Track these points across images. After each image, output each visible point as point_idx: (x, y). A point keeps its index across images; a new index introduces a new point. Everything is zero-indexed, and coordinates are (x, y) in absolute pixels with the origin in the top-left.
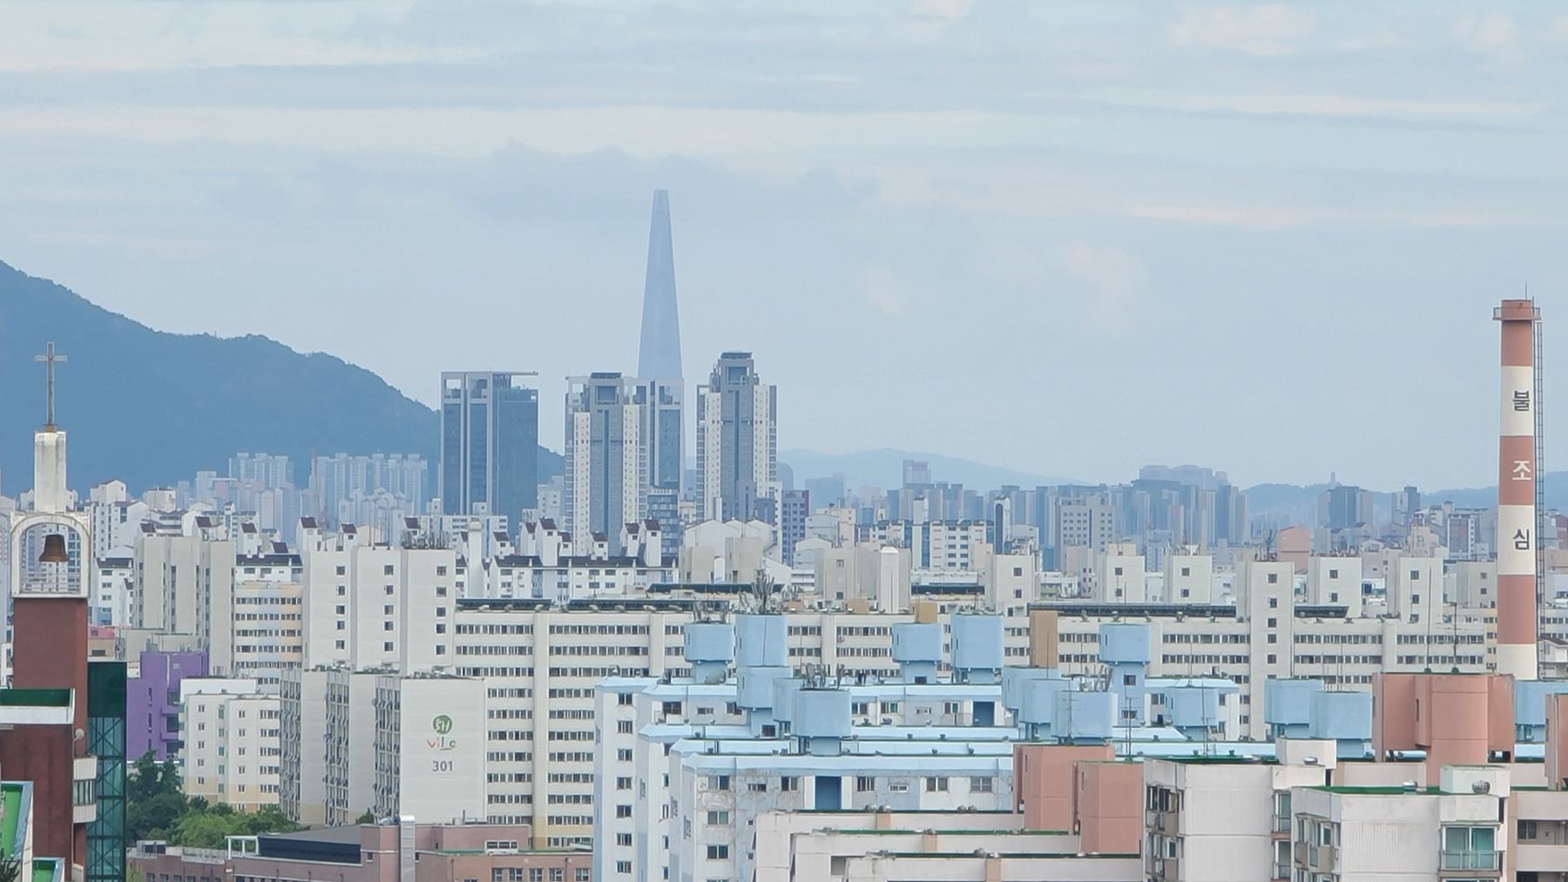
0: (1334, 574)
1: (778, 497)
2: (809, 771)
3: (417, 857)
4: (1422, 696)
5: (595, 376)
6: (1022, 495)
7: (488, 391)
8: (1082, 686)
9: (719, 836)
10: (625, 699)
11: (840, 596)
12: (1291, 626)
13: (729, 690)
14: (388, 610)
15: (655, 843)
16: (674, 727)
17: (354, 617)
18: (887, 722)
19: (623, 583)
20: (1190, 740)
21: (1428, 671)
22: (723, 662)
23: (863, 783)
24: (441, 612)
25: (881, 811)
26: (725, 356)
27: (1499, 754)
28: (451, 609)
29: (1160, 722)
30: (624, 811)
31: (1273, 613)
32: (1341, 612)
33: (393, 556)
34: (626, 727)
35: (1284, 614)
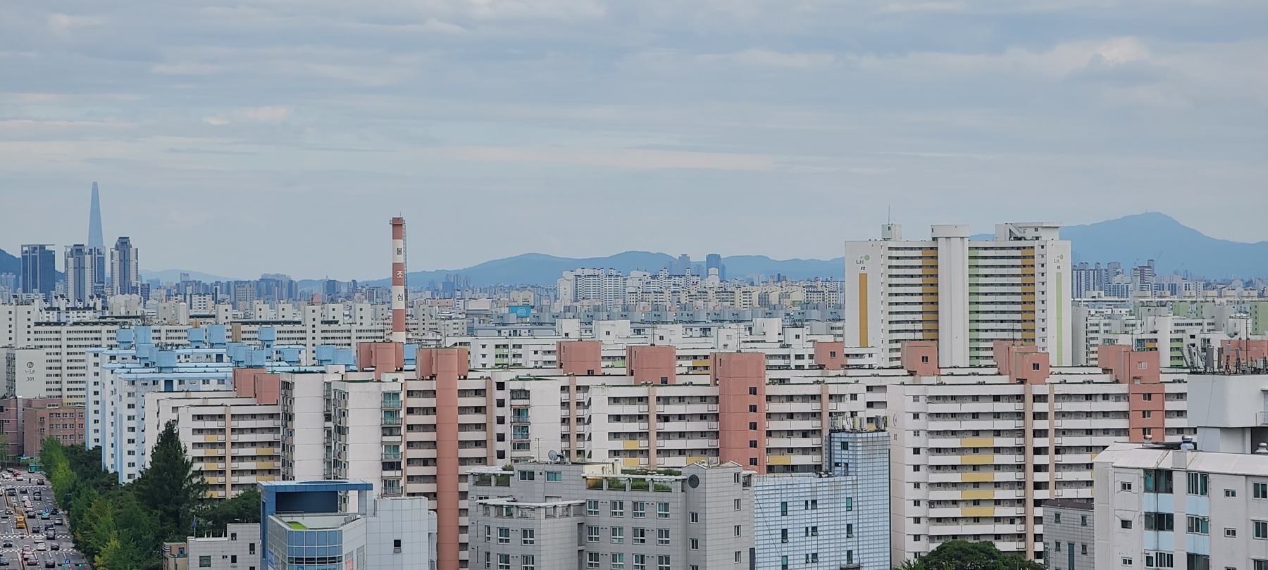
0: (361, 309)
1: (139, 286)
2: (163, 378)
3: (23, 410)
4: (373, 350)
5: (75, 245)
6: (222, 285)
7: (37, 251)
8: (255, 348)
9: (132, 401)
10: (96, 355)
11: (165, 319)
12: (320, 327)
13: (133, 352)
14: (10, 326)
15: (108, 404)
16: (114, 364)
17: (16, 329)
18: (187, 361)
19: (89, 316)
20: (291, 366)
21: (375, 341)
22: (130, 342)
23: (181, 382)
24: (29, 327)
25: (188, 391)
26: (120, 238)
27: (399, 369)
28: (32, 325)
29: (280, 360)
30: (96, 393)
31: (314, 323)
32: (336, 322)
33: (12, 308)
34: (96, 365)
35: (318, 323)
